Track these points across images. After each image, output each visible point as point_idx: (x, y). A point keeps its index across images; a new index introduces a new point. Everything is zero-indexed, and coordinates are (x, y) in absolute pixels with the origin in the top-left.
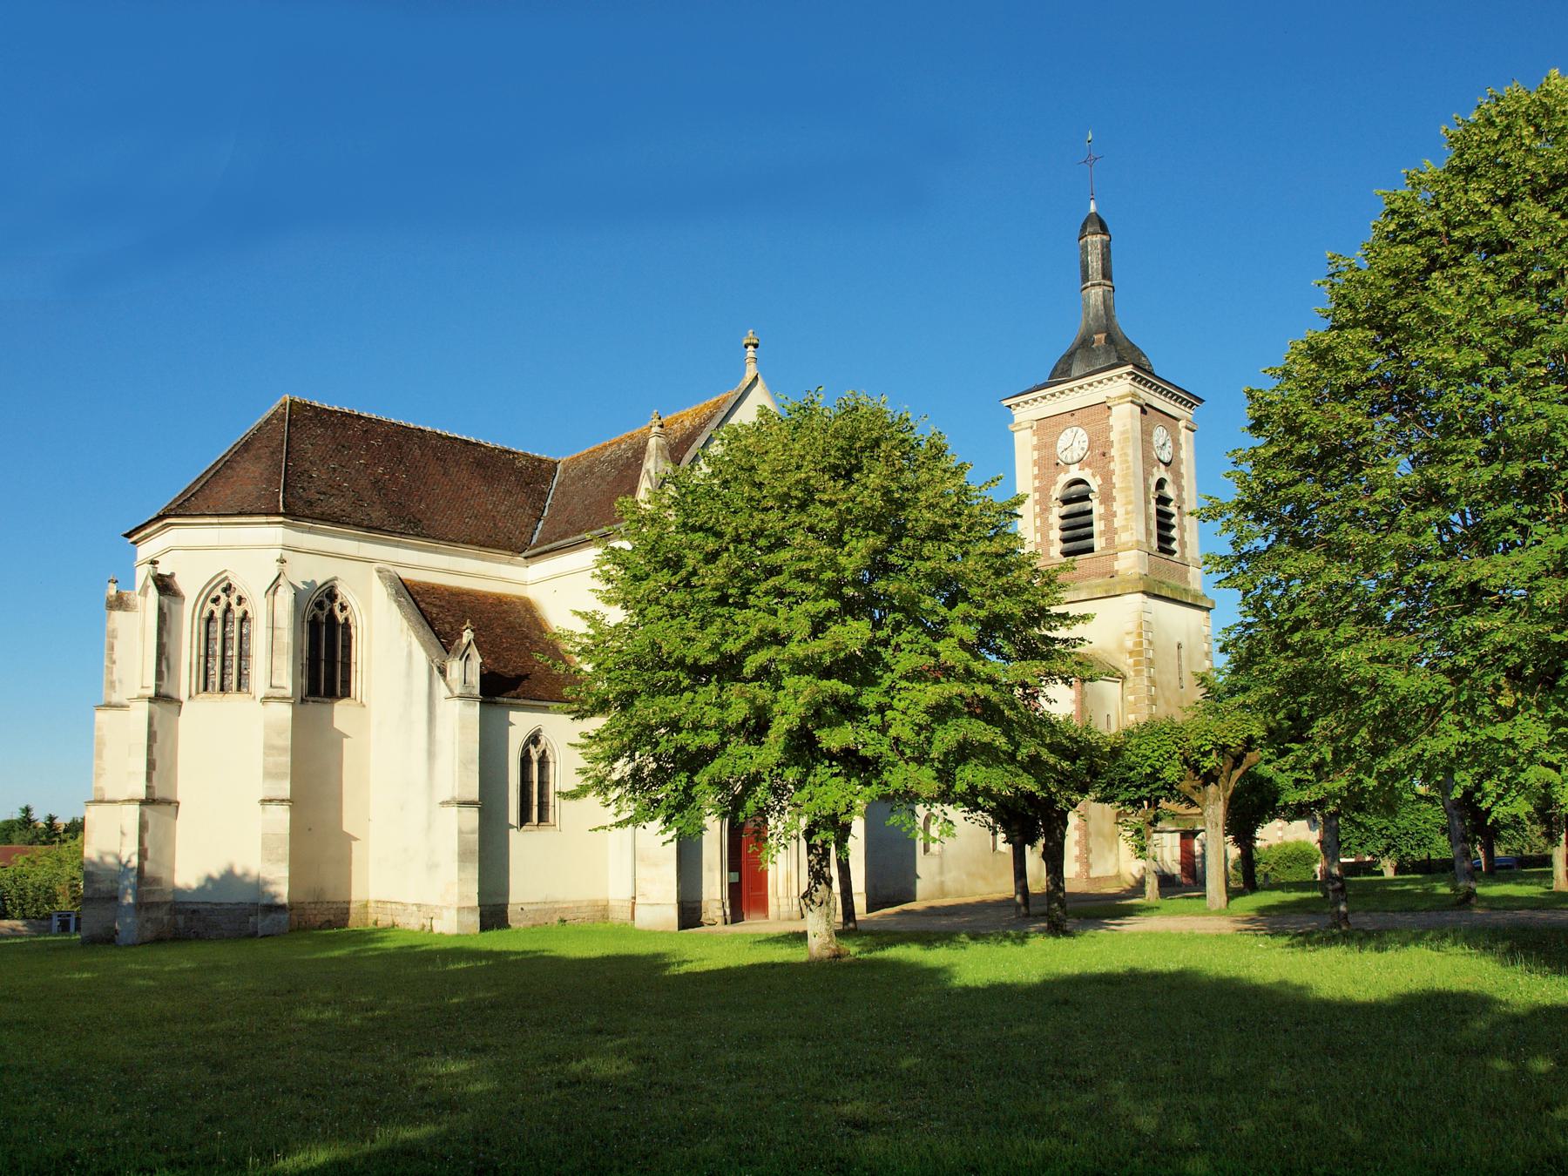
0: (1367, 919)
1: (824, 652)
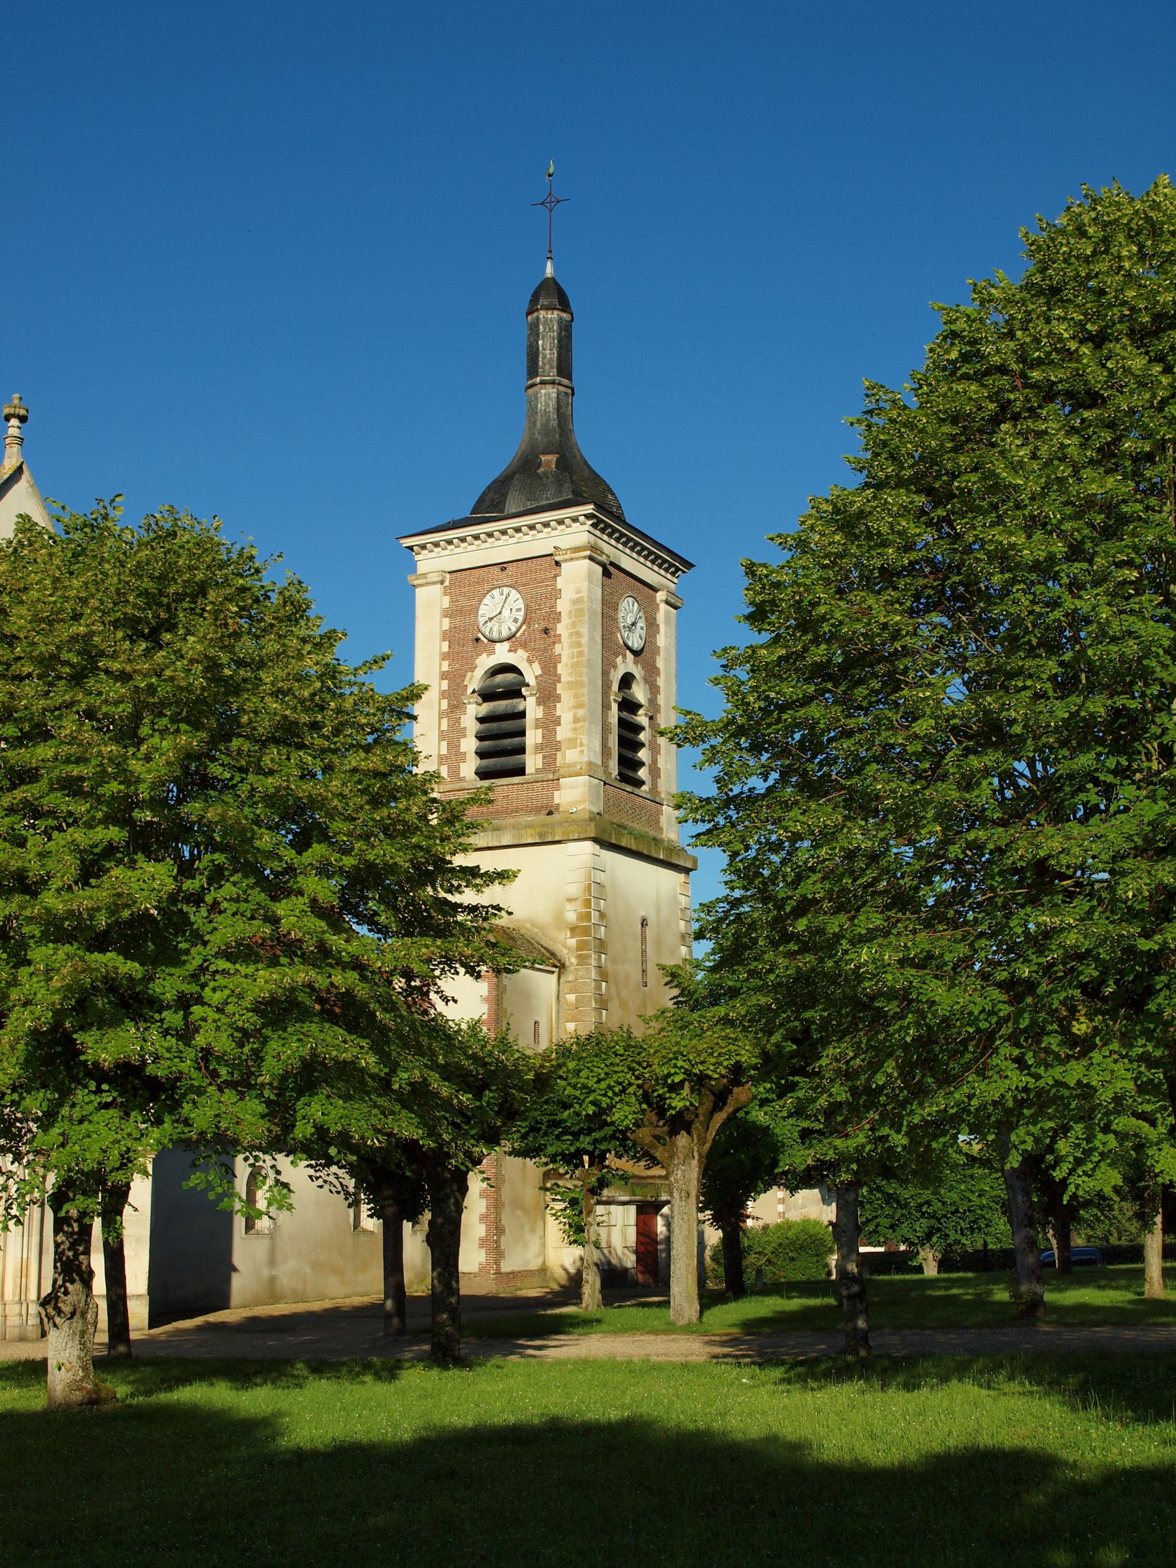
0: (895, 1339)
1: (99, 909)
